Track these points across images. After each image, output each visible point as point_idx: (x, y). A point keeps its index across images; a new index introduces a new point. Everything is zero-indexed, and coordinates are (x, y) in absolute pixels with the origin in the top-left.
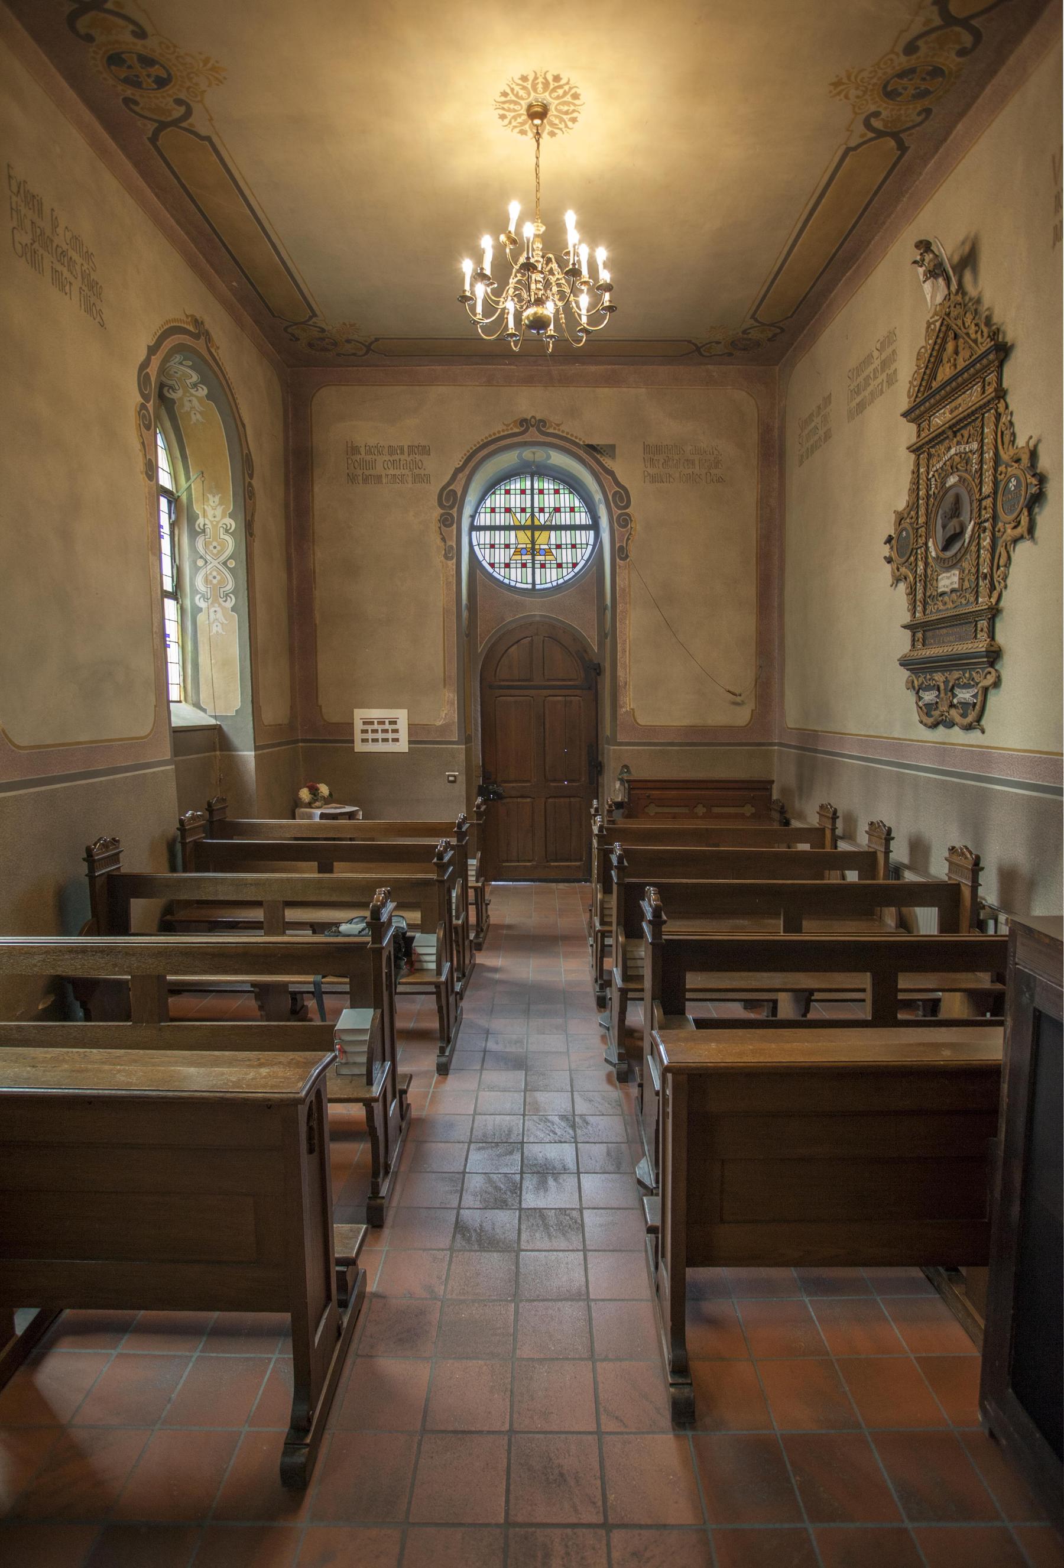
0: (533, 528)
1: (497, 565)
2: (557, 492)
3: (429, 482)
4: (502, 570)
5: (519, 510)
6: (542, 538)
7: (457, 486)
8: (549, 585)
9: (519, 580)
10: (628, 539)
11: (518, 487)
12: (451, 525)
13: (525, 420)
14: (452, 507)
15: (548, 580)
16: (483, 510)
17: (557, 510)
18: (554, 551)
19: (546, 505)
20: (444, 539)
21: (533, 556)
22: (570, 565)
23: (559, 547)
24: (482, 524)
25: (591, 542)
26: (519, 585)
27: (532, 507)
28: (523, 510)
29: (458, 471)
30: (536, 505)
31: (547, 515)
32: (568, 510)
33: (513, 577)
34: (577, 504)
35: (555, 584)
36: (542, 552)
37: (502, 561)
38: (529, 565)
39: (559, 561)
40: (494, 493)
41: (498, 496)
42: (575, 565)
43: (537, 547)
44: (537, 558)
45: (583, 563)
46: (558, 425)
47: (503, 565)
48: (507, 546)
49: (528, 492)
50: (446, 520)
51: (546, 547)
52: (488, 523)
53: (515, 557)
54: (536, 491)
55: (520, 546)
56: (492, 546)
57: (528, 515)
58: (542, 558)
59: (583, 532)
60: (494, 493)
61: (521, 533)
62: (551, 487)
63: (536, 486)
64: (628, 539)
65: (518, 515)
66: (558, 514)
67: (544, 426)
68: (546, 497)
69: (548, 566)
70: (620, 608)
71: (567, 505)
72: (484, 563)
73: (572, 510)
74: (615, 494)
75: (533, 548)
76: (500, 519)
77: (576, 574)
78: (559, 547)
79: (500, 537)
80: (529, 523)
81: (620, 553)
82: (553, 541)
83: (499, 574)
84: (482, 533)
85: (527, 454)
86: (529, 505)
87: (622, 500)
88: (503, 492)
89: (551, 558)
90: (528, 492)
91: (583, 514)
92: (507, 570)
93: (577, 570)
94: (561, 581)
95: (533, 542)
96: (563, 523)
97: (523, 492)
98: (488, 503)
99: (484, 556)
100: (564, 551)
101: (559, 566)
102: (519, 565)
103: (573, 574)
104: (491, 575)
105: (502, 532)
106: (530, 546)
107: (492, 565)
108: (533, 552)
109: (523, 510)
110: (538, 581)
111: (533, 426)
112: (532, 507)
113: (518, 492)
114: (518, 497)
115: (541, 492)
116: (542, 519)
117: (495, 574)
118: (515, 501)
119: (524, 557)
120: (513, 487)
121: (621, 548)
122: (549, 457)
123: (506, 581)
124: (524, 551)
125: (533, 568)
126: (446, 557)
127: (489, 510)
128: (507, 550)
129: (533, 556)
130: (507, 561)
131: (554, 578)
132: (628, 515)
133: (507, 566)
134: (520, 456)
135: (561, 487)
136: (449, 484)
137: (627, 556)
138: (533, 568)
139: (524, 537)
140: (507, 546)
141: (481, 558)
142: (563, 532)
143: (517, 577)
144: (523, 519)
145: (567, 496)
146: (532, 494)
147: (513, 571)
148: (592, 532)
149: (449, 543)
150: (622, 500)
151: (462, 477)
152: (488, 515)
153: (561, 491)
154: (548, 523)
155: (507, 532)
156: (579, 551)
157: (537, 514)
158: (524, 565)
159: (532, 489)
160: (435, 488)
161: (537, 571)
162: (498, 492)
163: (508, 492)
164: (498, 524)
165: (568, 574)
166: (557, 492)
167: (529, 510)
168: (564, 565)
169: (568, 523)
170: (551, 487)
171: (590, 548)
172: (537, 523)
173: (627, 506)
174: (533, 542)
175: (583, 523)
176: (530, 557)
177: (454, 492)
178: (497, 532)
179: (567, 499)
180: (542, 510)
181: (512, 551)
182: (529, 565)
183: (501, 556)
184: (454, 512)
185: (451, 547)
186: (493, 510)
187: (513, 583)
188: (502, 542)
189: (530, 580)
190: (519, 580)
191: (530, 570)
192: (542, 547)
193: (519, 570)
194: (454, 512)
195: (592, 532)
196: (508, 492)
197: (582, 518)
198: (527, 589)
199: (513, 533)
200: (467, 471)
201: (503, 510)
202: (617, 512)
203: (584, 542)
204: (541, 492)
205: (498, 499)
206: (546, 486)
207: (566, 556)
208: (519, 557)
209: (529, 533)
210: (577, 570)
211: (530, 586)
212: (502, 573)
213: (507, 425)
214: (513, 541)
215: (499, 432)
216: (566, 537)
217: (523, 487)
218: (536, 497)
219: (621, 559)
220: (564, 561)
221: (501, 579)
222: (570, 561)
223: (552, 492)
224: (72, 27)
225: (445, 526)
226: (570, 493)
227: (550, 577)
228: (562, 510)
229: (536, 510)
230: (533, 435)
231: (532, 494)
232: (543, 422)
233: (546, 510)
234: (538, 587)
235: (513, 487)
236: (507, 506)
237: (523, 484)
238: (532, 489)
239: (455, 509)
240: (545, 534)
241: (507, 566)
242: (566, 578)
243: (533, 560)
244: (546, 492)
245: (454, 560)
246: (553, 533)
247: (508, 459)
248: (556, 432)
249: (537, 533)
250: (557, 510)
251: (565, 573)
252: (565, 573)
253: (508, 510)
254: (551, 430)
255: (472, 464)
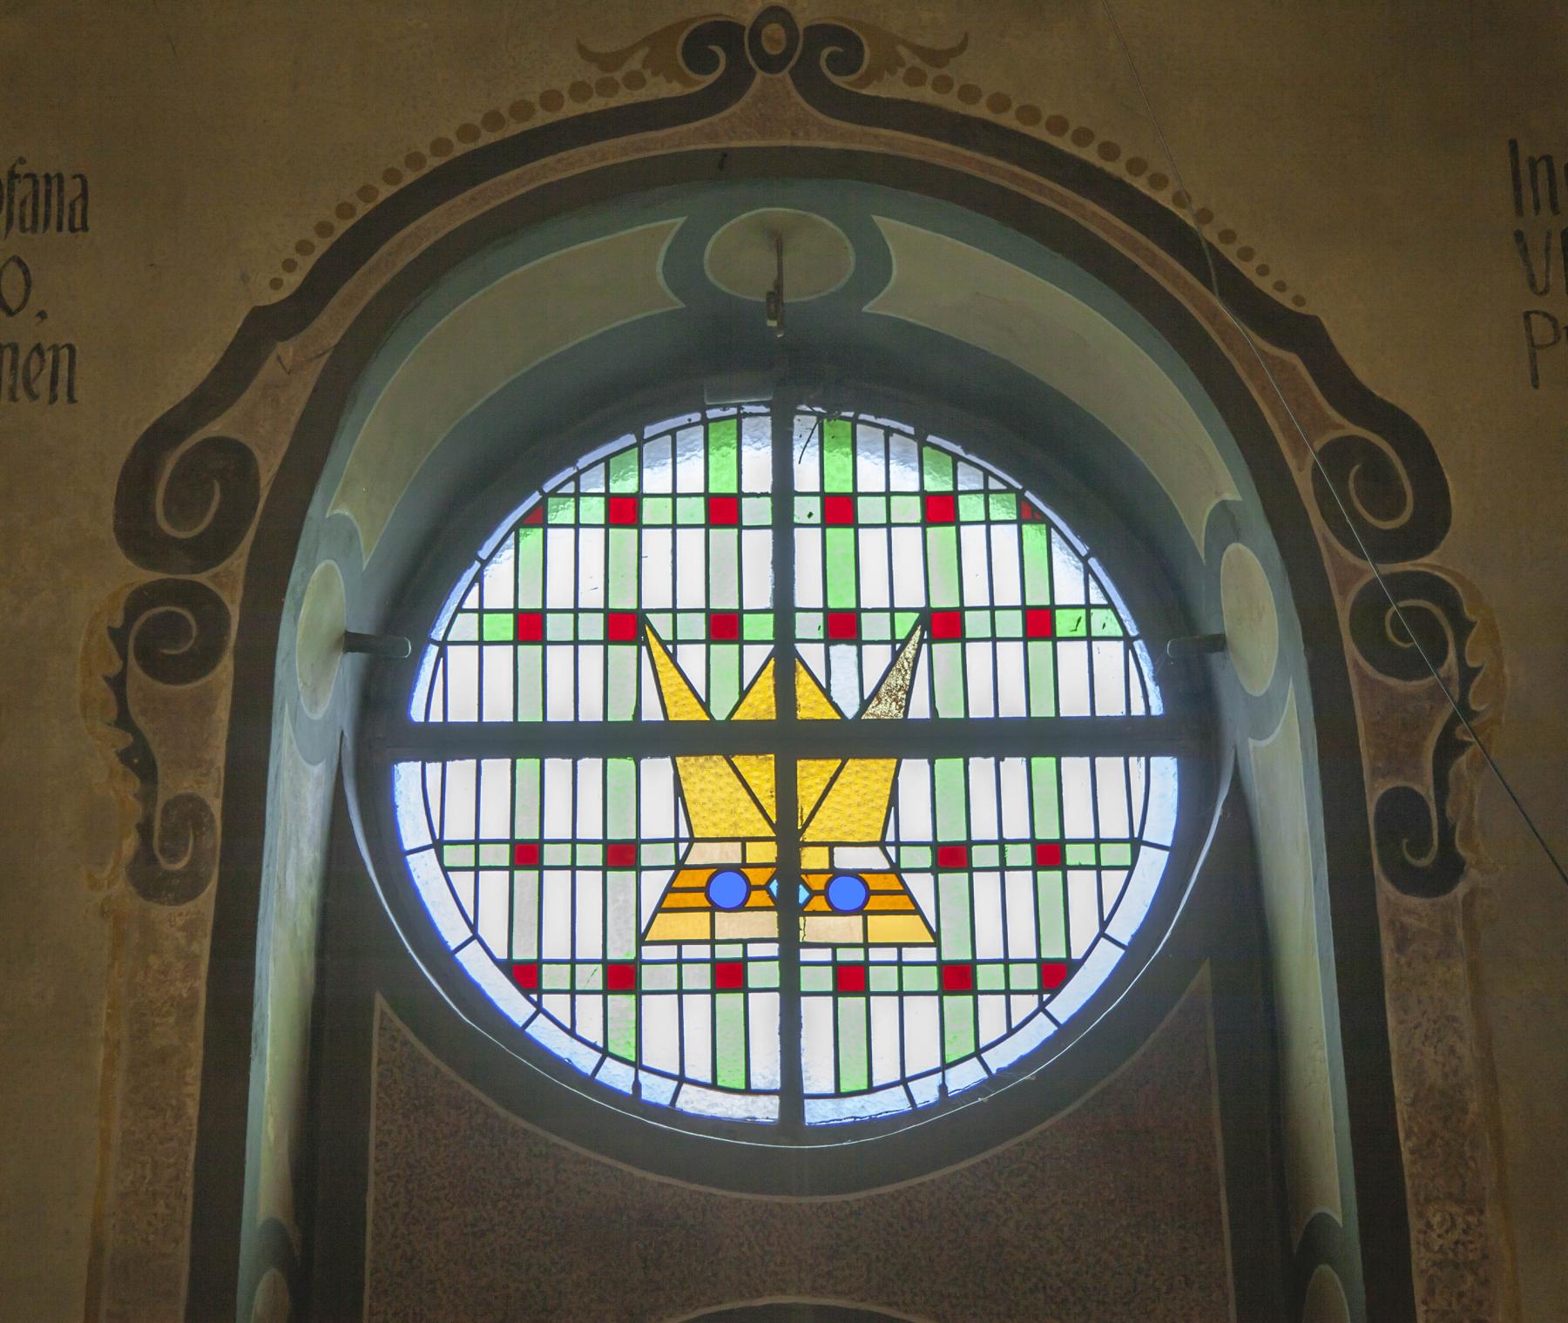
0: (789, 739)
1: (552, 977)
2: (939, 510)
3: (63, 389)
4: (590, 1008)
5: (696, 626)
6: (847, 806)
7: (263, 426)
8: (894, 1102)
9: (698, 1068)
10: (1449, 748)
11: (691, 476)
12: (204, 660)
13: (725, 32)
14: (211, 549)
15: (886, 1071)
16: (466, 627)
17: (944, 625)
18: (921, 886)
19: (873, 595)
20: (140, 762)
21: (789, 912)
22: (1027, 977)
23: (951, 857)
24: (462, 711)
25: (1162, 825)
26: (694, 1101)
27: (784, 607)
28: (724, 627)
29: (266, 327)
30: (807, 592)
31: (877, 658)
32: (1012, 624)
33: (660, 1053)
34: (1070, 585)
35: (925, 1093)
36: (847, 893)
37: (590, 947)
38: (763, 974)
39: (955, 951)
40: (537, 518)
41: (560, 541)
42: (1054, 975)
43: (813, 859)
44: (814, 928)
45: (1106, 959)
46: (935, 57)
47: (592, 977)
48: (622, 855)
49: (757, 511)
50: (171, 628)
51: (872, 859)
52: (498, 711)
53: (669, 926)
54: (807, 509)
55: (702, 854)
56: (527, 855)
57: (756, 656)
58: (846, 928)
59: (1111, 767)
60: (537, 518)
61: (709, 777)
62: (905, 478)
63: (805, 475)
64: (1449, 748)
65: (692, 658)
66: (946, 652)
67: (848, 62)
68: (873, 541)
69: (880, 978)
70: (1429, 1234)
71: (1008, 594)
72: (475, 964)
73: (1039, 623)
74: (1337, 455)
75: (788, 869)
76: (578, 682)
77: (1064, 1031)
78: (951, 857)
79: (574, 799)
80: (761, 705)
81: (1388, 843)
82: (914, 823)
83: (570, 1030)
84: (461, 770)
85: (738, 252)
86: (759, 592)
87: (1377, 474)
88: (594, 510)
89: (908, 928)
90: (757, 511)
91: (1110, 656)
92: (622, 1003)
93: (1068, 1002)
94: (965, 1077)
95: (788, 829)
96: (981, 708)
97: (723, 511)
98: (498, 583)
99: (471, 916)
100: (986, 884)
101: (958, 978)
102: (699, 977)
103: (1042, 1029)
104: (517, 1035)
105: (590, 767)
106: (765, 853)
107: (526, 976)
108: (788, 891)
109: (724, 627)
110: (817, 1076)
111: (771, 64)
112: (784, 607)
113: (694, 511)
114: (692, 541)
115: (839, 510)
116: (843, 681)
117: (542, 1032)
118: (674, 569)
119: (730, 925)
120: (657, 479)
121: (1402, 807)
122: (874, 266)
123: (617, 1076)
124: (728, 888)
125: (790, 994)
126: (149, 879)
127: (504, 627)
128: (621, 879)
129: (789, 912)
130: (623, 950)
131: (923, 1055)
132: (1432, 587)
133: (622, 978)
134: (684, 265)
135: (969, 479)
136: (204, 402)
137: (1449, 869)
138: (790, 994)
139: (726, 803)
140: (622, 855)
141: (452, 930)
142: (982, 767)
143: (690, 1055)
144: (731, 682)
145: (1005, 537)
146: (783, 527)
147: (659, 1011)
148: (1166, 769)
149: (175, 784)
150: (1382, 493)
151: (293, 368)
152: (499, 660)
153: (970, 507)
154: (884, 709)
155: (621, 767)
156: (1082, 883)
157: (812, 654)
158: (729, 976)
159: (783, 492)
160: (99, 433)
161: (816, 1013)
162: (561, 512)
163: (624, 511)
164: (560, 711)
165: (1012, 1031)
166: (939, 510)
167: (759, 627)
168: (988, 977)
169: (1012, 707)
170: (905, 478)
171: (1153, 865)
172: (811, 706)
173: (1430, 526)
174: (788, 829)
175: (1111, 705)
176: (766, 923)
177: (237, 459)
178: (558, 768)
179: (1009, 554)
180: (843, 626)
181: (654, 884)
182: (763, 974)
183: (578, 916)
184: (229, 581)
185: (190, 812)
186: (530, 627)
187: (657, 1091)
188: (590, 827)
189: (767, 1071)
190: (698, 1068)
191: (765, 1009)
192: (847, 859)
193: (698, 1007)
194: (229, 581)
195: (1166, 769)
196: (624, 511)
197: (1105, 672)
198: (749, 1127)
199: (657, 772)
200: (330, 327)
201: (594, 627)
202: (1353, 572)
203: (1114, 825)
204: (839, 510)
205: (557, 557)
206: (871, 474)
207: (1000, 916)
208: (696, 925)
209: (761, 771)
210: (1068, 1002)
211: (766, 1110)
212: (590, 1027)
213: (608, 62)
214: (658, 820)
215: (551, 99)
216: (998, 798)
217: (723, 484)
218: (807, 543)
219: (1409, 880)
220: (989, 947)
221: (585, 1060)
222: (1023, 946)
223: (912, 509)
224: (80, 176)
225: (156, 667)
226: (1027, 514)
227: (896, 1057)
228: (975, 624)
229: (809, 626)
230: (772, 114)
231: (783, 527)
232: (842, 42)
233: (873, 626)
234: (817, 1113)
235: (657, 479)
236: (623, 601)
237: (723, 458)
238: (783, 492)
239: (238, 562)
240: (865, 778)
241: (622, 978)
242: (999, 1059)
243: (790, 943)
244: (869, 510)
245: (206, 902)
246: (914, 772)
247: (607, 278)
248: (926, 94)
249: (812, 775)
250: (944, 625)
251: (992, 1026)
252: (992, 1026)
253: (625, 627)
254: (891, 88)
255: (365, 286)
